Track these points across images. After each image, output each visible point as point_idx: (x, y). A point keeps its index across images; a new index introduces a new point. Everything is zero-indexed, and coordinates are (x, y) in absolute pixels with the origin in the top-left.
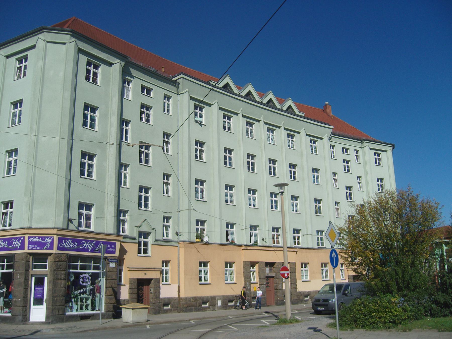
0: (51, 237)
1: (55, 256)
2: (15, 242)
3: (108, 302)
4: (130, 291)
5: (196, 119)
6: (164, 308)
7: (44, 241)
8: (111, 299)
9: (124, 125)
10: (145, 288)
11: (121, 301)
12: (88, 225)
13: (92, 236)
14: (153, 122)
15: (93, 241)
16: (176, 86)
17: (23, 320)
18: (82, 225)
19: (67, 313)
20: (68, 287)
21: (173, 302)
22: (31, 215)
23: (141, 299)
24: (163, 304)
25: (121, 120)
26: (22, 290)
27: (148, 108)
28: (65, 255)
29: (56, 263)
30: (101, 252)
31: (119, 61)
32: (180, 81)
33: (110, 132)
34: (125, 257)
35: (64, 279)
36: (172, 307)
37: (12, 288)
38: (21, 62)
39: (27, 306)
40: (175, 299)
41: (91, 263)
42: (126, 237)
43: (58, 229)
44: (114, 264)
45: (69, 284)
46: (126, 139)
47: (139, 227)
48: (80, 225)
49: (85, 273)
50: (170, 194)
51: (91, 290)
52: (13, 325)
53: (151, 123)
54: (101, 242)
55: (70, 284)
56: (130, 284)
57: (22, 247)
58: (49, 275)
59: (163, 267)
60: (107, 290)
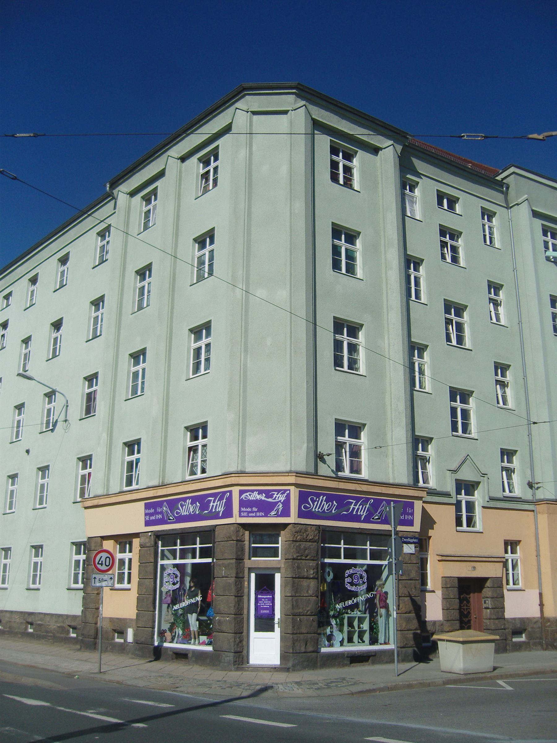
0: (285, 491)
1: (294, 530)
2: (214, 502)
3: (404, 625)
4: (445, 603)
5: (548, 253)
6: (514, 640)
7: (270, 500)
8: (408, 620)
9: (410, 269)
10: (473, 597)
11: (427, 623)
12: (355, 469)
13: (365, 488)
14: (467, 260)
15: (368, 500)
16: (502, 192)
17: (236, 662)
18: (343, 468)
19: (322, 649)
20: (323, 594)
21: (532, 628)
22: (243, 447)
23: (466, 620)
24: (511, 631)
25: (406, 259)
26: (232, 600)
27: (455, 235)
28: (313, 528)
29: (298, 544)
30: (391, 523)
31: (391, 142)
32: (510, 180)
33: (387, 279)
34: (431, 533)
35: (312, 578)
36: (530, 637)
37: (212, 595)
38: (207, 163)
39: (242, 633)
40: (535, 620)
41: (366, 546)
42: (432, 492)
43: (299, 474)
44: (412, 546)
45: (323, 587)
46: (418, 296)
47: (455, 471)
48: (339, 467)
49: (355, 565)
50: (511, 404)
51: (367, 600)
52: (217, 670)
53: (462, 263)
54: (384, 502)
55: (325, 589)
56: (445, 589)
57: (228, 513)
58: (283, 570)
59: (506, 555)
60: (400, 602)
